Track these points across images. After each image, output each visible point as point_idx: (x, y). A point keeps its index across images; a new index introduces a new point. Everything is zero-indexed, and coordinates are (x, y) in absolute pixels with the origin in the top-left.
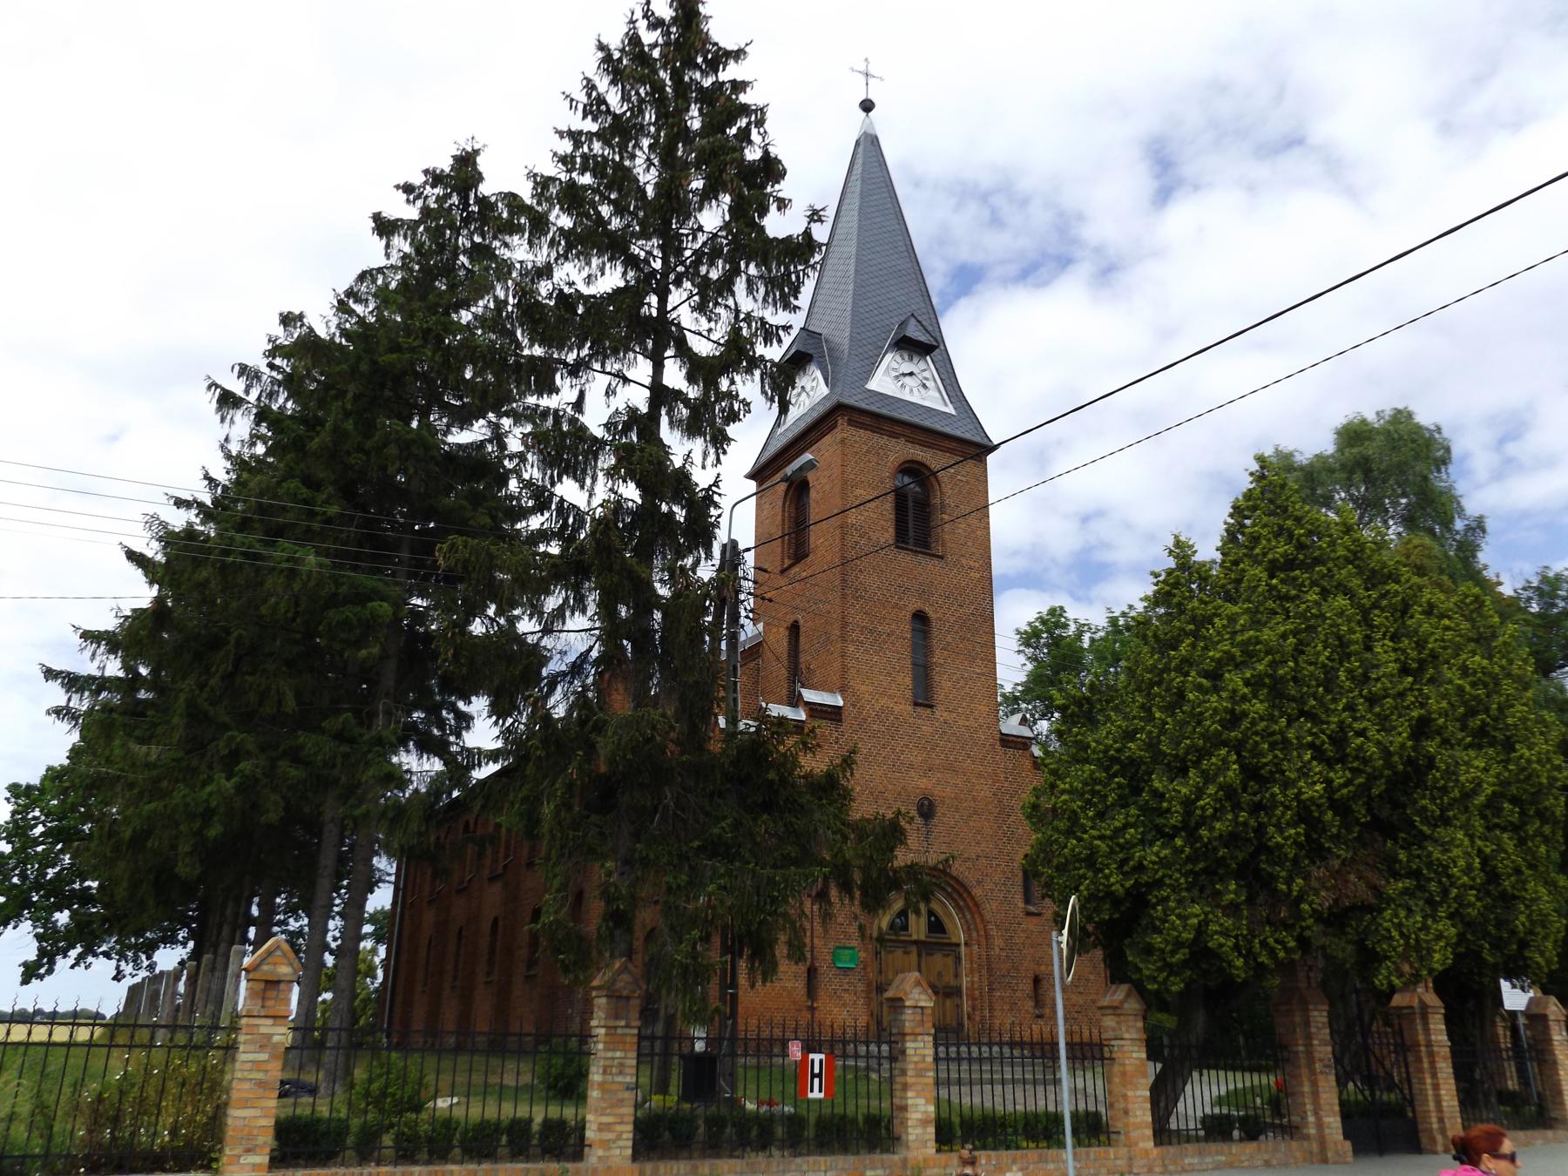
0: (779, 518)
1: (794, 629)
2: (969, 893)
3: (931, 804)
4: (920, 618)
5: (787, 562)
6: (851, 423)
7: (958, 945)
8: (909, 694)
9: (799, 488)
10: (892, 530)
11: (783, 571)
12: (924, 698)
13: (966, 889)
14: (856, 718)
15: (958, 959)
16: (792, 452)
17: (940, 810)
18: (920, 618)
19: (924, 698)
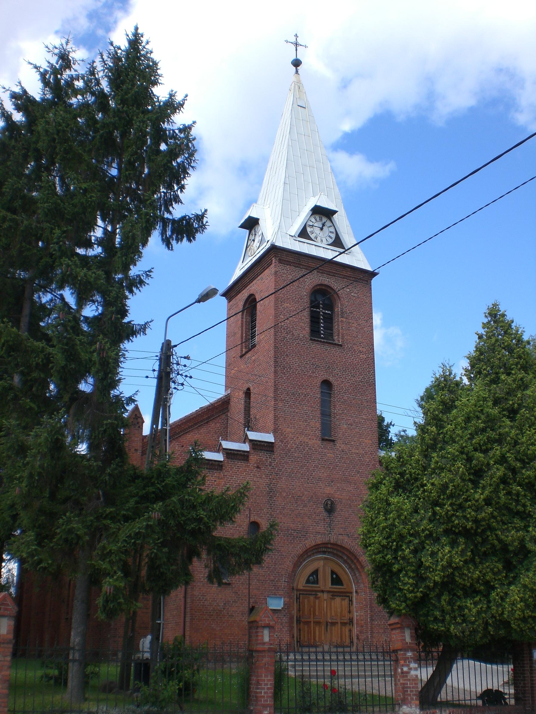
0: (240, 322)
1: (248, 393)
2: (358, 560)
3: (332, 503)
4: (327, 384)
5: (244, 351)
6: (281, 261)
7: (351, 593)
8: (318, 433)
9: (251, 303)
10: (308, 329)
11: (241, 357)
12: (327, 437)
13: (355, 557)
14: (283, 450)
15: (351, 601)
16: (247, 280)
17: (339, 507)
18: (327, 384)
19: (327, 437)
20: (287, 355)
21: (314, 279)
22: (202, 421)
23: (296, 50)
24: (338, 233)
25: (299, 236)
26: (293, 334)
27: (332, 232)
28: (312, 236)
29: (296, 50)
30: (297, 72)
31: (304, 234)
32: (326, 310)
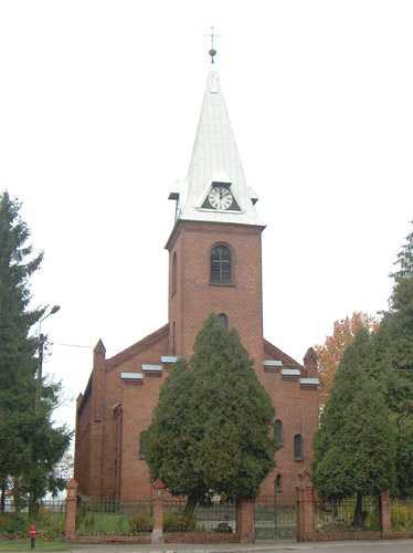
21: (210, 240)
31: (206, 205)
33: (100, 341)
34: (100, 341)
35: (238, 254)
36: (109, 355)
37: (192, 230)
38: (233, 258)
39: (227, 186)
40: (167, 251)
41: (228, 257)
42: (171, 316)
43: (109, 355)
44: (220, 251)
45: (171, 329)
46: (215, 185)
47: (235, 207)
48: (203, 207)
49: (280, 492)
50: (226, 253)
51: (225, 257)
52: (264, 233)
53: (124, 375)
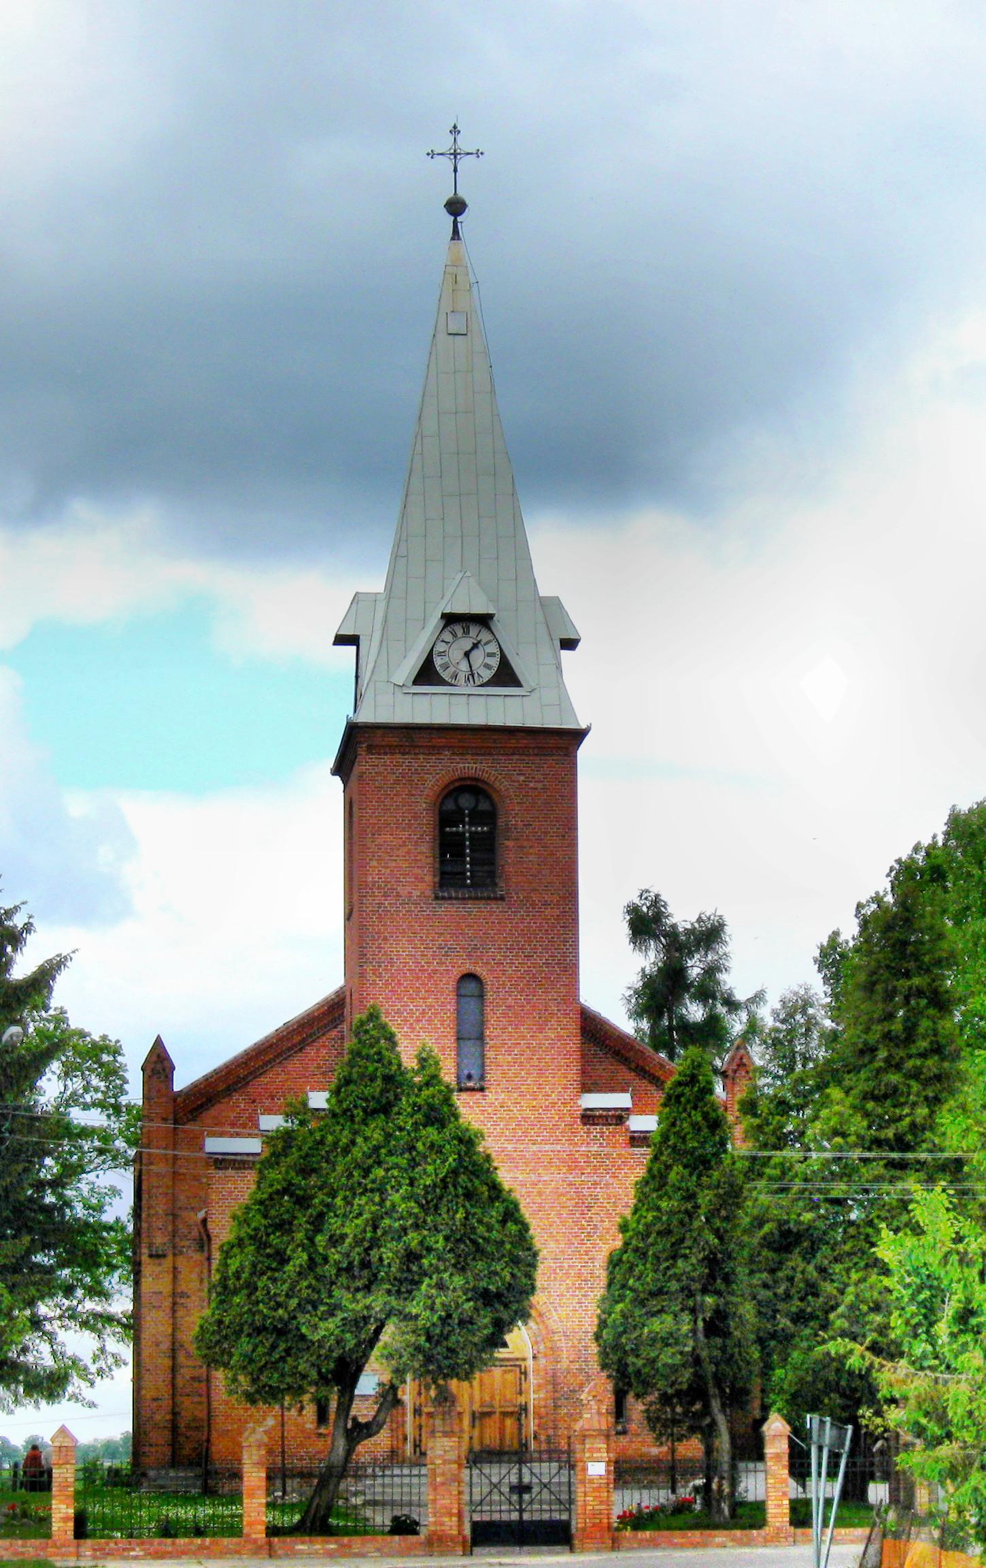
20: (385, 939)
21: (438, 771)
22: (289, 1049)
23: (455, 170)
24: (506, 653)
25: (415, 682)
26: (398, 895)
27: (491, 655)
28: (446, 675)
29: (455, 170)
30: (456, 234)
31: (427, 674)
32: (477, 825)
33: (158, 1043)
34: (158, 1043)
35: (513, 815)
36: (182, 1080)
37: (390, 750)
38: (501, 822)
39: (484, 621)
40: (337, 779)
41: (489, 817)
42: (346, 980)
43: (182, 1080)
44: (466, 801)
45: (348, 1000)
46: (450, 619)
47: (505, 676)
48: (417, 682)
49: (624, 1432)
50: (484, 806)
51: (477, 817)
52: (585, 753)
53: (214, 1145)
